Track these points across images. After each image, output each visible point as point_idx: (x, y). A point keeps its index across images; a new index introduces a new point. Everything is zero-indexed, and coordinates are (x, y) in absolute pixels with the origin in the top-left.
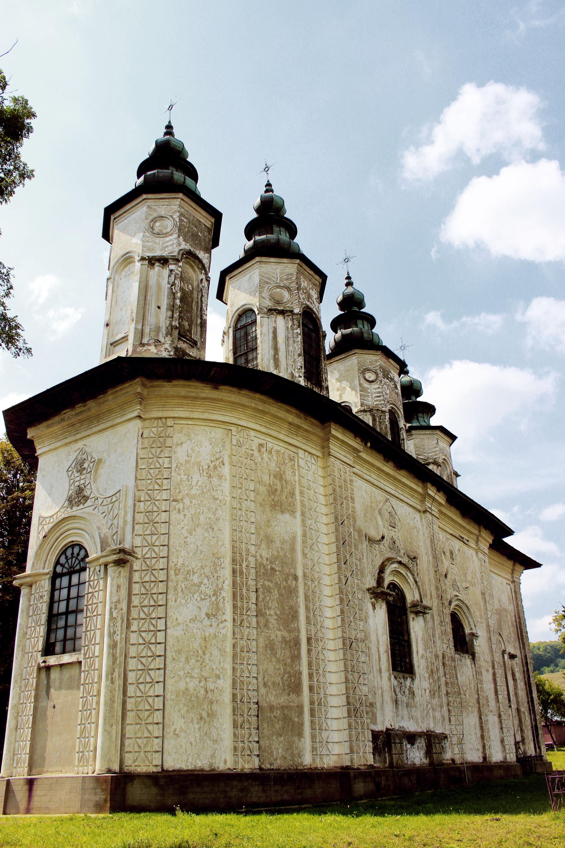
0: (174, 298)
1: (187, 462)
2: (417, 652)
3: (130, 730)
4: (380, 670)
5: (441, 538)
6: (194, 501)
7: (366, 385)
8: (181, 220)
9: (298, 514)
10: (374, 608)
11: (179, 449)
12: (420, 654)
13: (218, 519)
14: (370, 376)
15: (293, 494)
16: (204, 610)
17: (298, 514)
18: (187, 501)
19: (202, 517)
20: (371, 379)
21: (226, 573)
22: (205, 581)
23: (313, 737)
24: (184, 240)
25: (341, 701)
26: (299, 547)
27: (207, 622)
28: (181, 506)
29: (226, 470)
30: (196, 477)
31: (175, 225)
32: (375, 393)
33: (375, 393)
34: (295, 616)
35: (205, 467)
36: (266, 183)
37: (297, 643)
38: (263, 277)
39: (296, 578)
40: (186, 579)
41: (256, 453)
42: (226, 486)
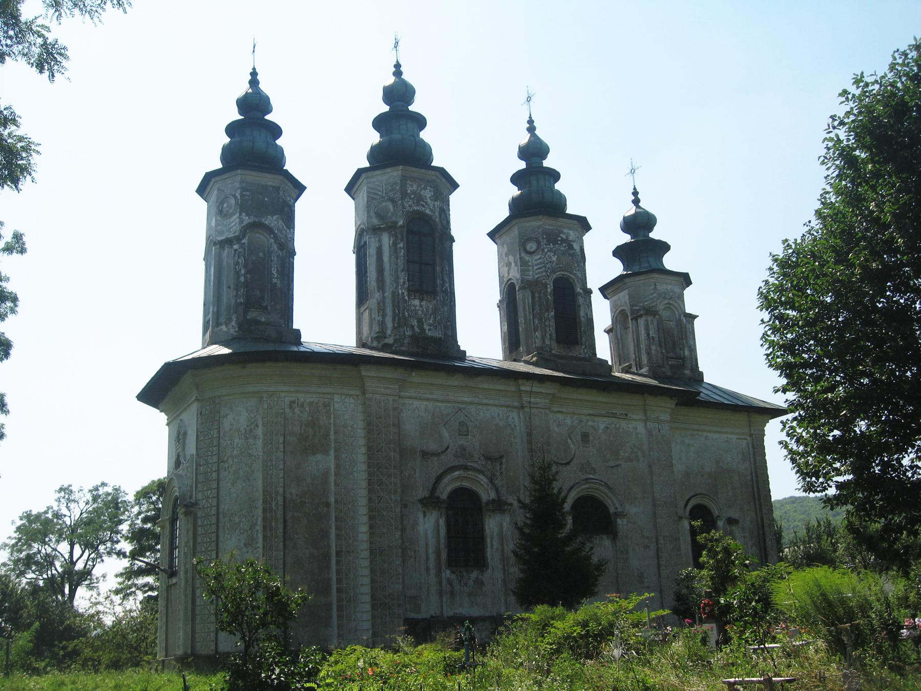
0: (238, 277)
1: (231, 429)
2: (492, 546)
3: (198, 627)
4: (428, 569)
5: (35, 576)
6: (236, 460)
7: (527, 258)
8: (242, 196)
9: (332, 452)
10: (425, 516)
11: (225, 420)
12: (495, 547)
13: (253, 472)
14: (532, 246)
15: (327, 435)
16: (243, 541)
17: (332, 452)
18: (230, 461)
19: (241, 472)
20: (532, 250)
21: (259, 512)
22: (244, 520)
23: (340, 627)
24: (247, 215)
25: (368, 598)
26: (332, 479)
27: (245, 550)
28: (226, 465)
29: (260, 431)
30: (236, 441)
31: (236, 204)
32: (537, 265)
33: (537, 265)
34: (325, 534)
35: (243, 431)
36: (395, 63)
37: (327, 557)
38: (370, 193)
39: (328, 505)
40: (230, 520)
41: (288, 410)
42: (260, 443)
